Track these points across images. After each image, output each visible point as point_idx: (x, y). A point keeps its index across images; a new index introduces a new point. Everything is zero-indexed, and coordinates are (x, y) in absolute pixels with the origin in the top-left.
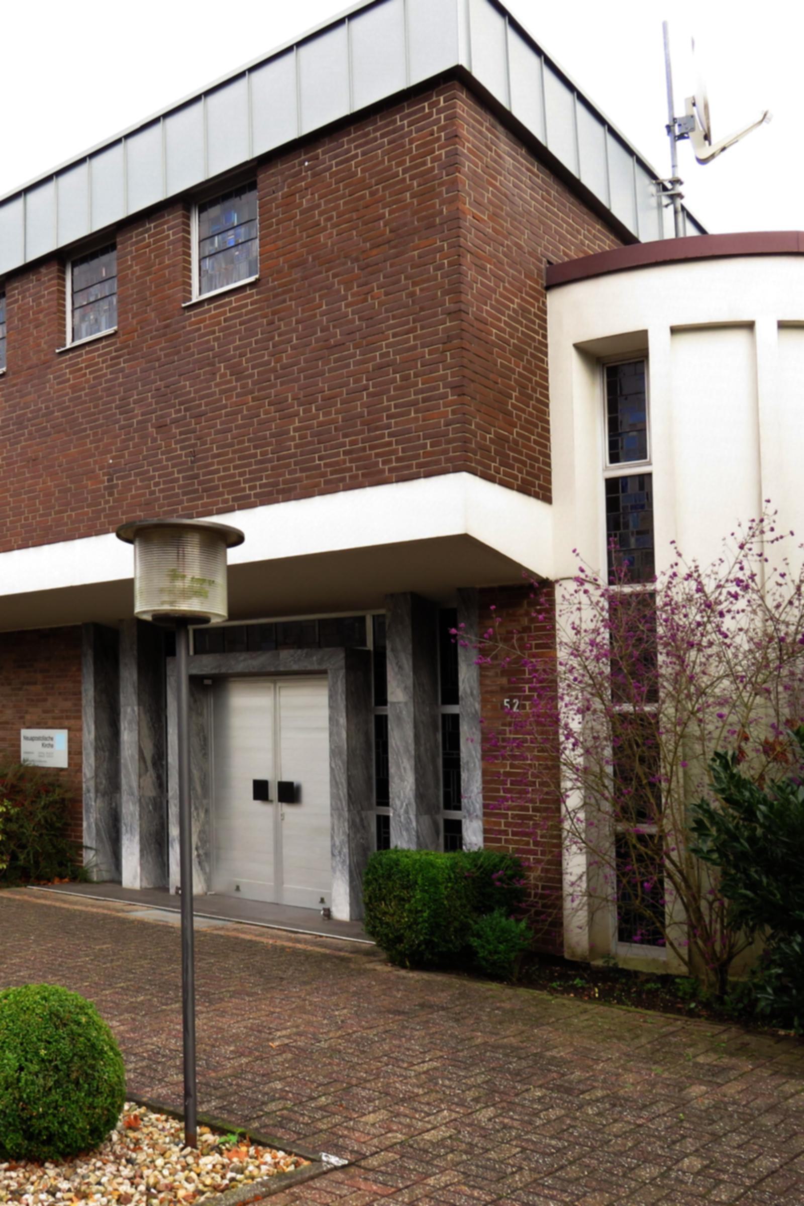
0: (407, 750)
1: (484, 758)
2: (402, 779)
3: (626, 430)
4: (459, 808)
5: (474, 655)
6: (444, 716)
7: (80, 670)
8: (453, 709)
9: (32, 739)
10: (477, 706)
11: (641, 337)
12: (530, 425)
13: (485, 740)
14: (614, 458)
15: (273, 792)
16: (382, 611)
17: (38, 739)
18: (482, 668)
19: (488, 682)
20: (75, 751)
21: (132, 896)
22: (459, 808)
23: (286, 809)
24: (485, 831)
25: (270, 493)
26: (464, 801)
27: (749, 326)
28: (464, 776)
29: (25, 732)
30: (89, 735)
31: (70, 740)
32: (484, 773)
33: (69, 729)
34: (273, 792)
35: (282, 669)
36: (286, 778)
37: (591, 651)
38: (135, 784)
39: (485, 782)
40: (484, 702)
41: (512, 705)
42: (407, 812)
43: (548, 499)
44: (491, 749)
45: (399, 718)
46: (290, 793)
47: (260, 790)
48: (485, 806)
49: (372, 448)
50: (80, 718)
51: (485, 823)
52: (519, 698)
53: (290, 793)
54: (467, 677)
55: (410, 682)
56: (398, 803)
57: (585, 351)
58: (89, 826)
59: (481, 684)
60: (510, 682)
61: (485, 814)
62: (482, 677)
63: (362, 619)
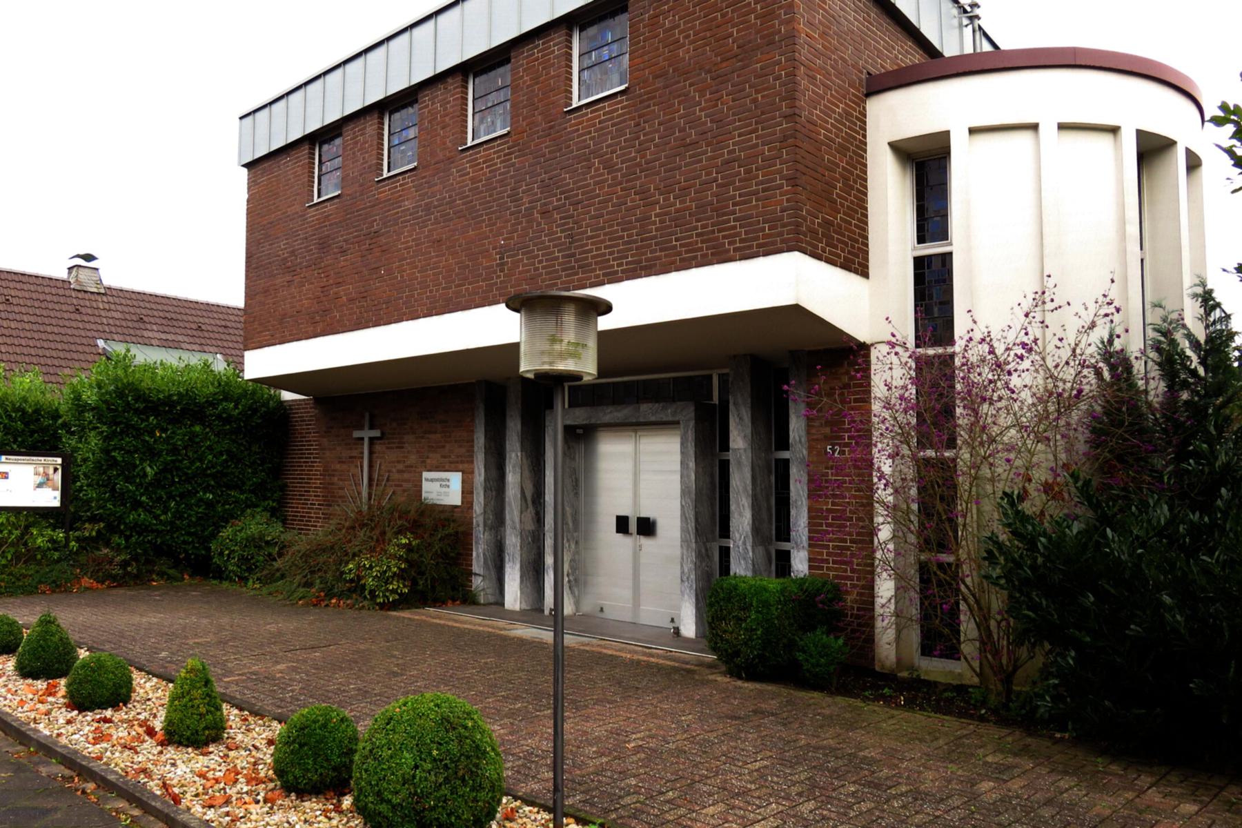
0: (745, 489)
1: (810, 496)
2: (741, 515)
4: (788, 540)
5: (802, 408)
7: (473, 420)
9: (432, 480)
10: (805, 452)
12: (851, 212)
13: (810, 481)
17: (437, 480)
20: (467, 491)
22: (788, 540)
24: (810, 560)
25: (634, 270)
28: (793, 512)
29: (426, 475)
30: (479, 477)
31: (463, 482)
32: (810, 510)
33: (463, 472)
35: (642, 420)
39: (810, 518)
40: (810, 449)
41: (834, 451)
42: (744, 543)
44: (816, 488)
45: (739, 463)
46: (647, 527)
48: (810, 538)
49: (719, 231)
50: (472, 462)
51: (810, 553)
52: (839, 445)
54: (796, 427)
56: (737, 535)
58: (478, 556)
59: (808, 433)
60: (832, 431)
61: (810, 545)
62: (809, 427)
63: (710, 377)
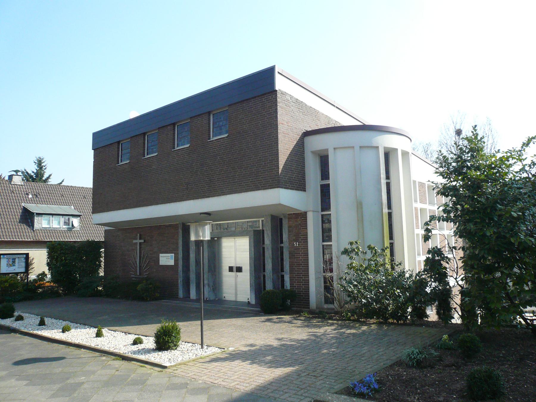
3: (325, 174)
6: (281, 247)
8: (282, 245)
11: (327, 150)
14: (322, 179)
15: (235, 269)
16: (263, 219)
18: (289, 235)
19: (291, 223)
20: (176, 260)
21: (193, 301)
23: (238, 274)
26: (285, 270)
27: (353, 147)
29: (161, 255)
30: (180, 256)
34: (235, 269)
36: (238, 266)
37: (468, 157)
38: (194, 269)
40: (290, 244)
43: (305, 191)
46: (239, 269)
47: (231, 269)
53: (239, 269)
55: (271, 239)
57: (314, 153)
59: (289, 239)
